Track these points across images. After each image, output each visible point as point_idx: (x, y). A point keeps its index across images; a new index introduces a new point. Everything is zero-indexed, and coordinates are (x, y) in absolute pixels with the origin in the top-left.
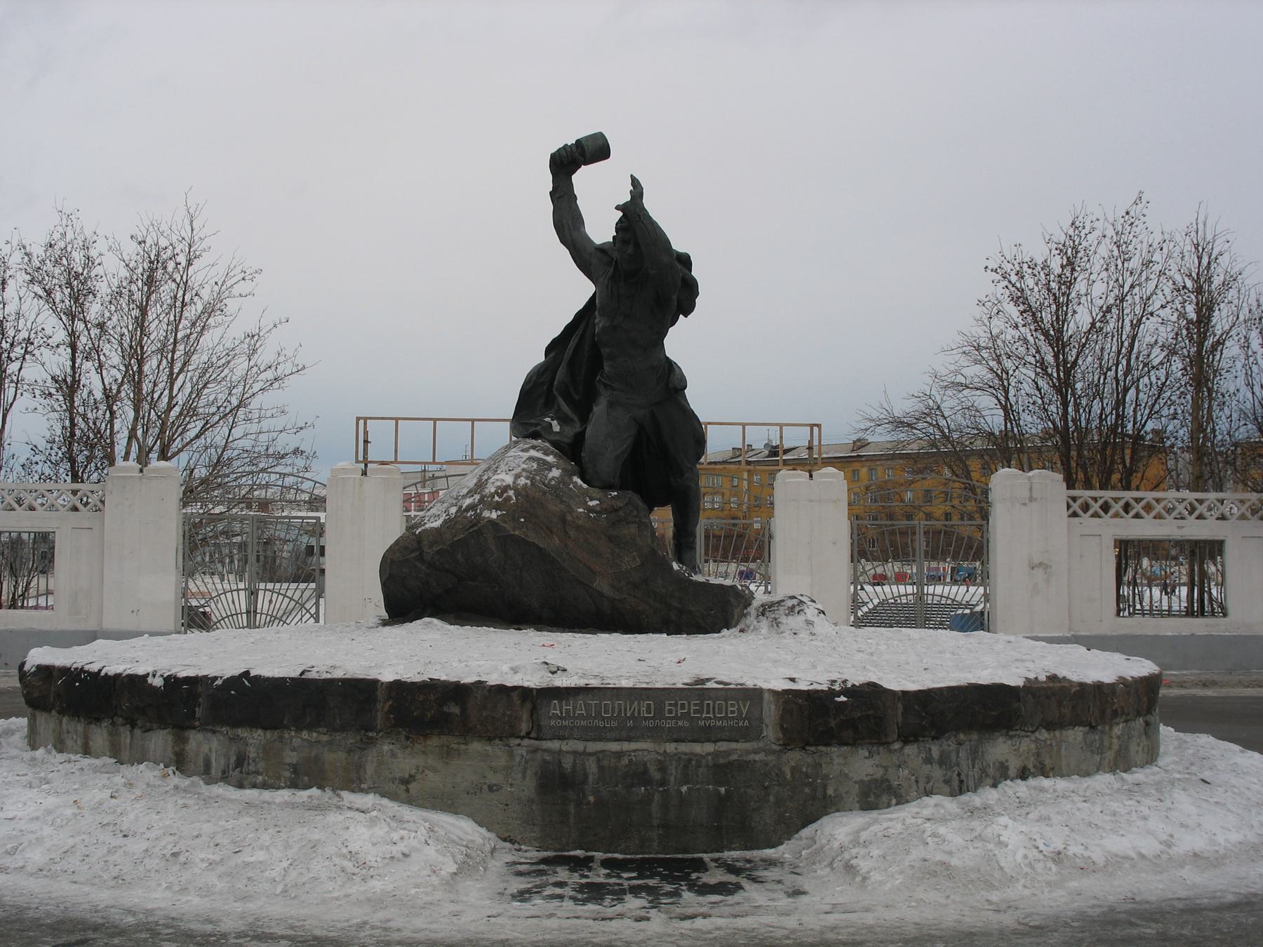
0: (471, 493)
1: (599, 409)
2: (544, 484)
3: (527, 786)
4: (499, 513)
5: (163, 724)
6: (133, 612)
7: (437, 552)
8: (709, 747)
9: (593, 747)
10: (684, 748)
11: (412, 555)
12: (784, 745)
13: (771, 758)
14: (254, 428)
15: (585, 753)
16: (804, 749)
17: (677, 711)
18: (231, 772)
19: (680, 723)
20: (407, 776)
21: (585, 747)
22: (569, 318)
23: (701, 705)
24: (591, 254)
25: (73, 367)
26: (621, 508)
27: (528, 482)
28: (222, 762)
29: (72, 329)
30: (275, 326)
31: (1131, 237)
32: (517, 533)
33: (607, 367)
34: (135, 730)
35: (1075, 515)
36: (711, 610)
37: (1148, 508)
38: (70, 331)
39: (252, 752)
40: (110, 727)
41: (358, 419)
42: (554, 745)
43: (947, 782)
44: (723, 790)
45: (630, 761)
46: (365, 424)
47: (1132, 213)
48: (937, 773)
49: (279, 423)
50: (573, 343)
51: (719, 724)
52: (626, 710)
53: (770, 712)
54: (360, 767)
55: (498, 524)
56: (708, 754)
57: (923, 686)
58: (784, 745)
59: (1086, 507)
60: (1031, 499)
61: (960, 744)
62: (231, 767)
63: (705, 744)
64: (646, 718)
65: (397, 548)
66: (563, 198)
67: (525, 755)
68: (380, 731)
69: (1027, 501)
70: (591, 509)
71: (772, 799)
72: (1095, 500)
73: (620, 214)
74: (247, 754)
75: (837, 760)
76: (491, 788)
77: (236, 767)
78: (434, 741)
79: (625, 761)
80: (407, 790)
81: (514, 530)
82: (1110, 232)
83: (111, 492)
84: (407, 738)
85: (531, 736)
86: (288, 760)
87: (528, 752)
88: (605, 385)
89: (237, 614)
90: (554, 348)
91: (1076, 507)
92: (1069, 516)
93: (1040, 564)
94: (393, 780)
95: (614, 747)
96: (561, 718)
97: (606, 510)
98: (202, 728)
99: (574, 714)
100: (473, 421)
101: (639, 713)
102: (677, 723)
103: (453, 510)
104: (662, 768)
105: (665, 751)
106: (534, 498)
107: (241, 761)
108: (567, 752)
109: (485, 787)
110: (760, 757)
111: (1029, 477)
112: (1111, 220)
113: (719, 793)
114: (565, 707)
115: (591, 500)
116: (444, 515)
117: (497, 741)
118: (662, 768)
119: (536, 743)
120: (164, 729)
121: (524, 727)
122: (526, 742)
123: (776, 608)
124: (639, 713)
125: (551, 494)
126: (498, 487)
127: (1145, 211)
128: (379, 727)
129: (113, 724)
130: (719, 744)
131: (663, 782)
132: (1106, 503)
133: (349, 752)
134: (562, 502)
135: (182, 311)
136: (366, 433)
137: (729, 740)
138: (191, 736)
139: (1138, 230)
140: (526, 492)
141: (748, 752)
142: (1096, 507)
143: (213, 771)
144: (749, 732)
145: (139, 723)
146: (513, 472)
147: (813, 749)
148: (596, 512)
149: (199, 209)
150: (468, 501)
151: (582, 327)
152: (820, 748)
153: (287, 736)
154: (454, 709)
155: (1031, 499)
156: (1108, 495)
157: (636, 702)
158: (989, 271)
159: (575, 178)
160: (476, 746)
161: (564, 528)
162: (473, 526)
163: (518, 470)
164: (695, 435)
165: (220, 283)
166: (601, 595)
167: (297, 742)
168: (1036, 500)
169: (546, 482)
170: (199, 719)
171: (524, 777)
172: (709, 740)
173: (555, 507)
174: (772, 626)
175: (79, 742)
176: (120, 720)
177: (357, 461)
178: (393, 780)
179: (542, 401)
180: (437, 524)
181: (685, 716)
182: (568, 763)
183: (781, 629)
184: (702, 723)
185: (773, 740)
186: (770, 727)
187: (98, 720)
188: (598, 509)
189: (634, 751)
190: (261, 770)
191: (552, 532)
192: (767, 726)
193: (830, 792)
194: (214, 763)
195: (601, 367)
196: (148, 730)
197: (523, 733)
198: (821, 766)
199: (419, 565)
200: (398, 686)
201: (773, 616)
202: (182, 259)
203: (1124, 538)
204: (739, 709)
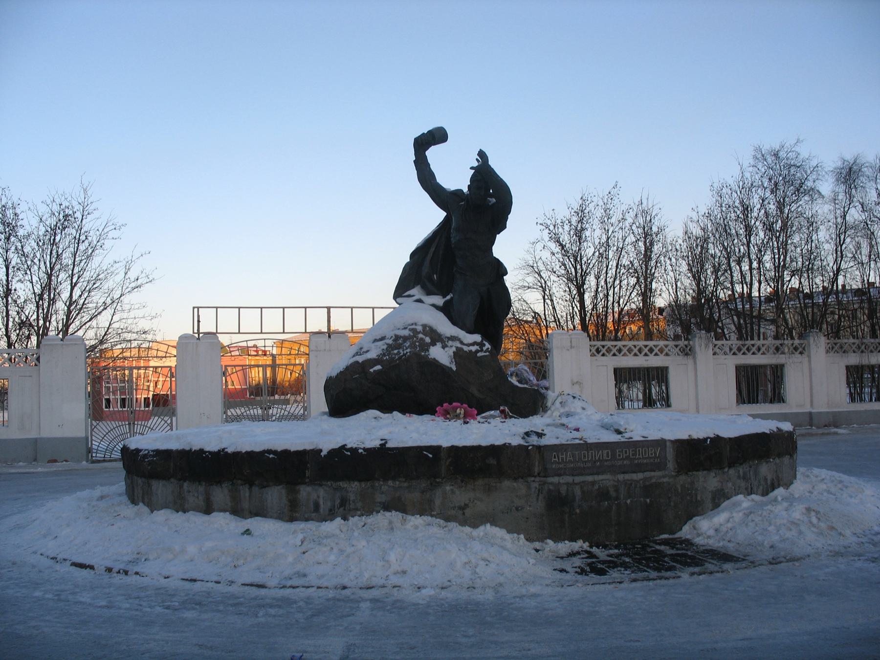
3: (538, 506)
5: (278, 481)
6: (59, 426)
8: (640, 476)
9: (578, 479)
10: (627, 477)
12: (677, 472)
13: (672, 480)
14: (125, 315)
15: (575, 484)
16: (687, 473)
17: (623, 455)
18: (336, 511)
19: (625, 462)
20: (463, 504)
21: (573, 480)
25: (7, 280)
28: (329, 504)
29: (6, 257)
30: (142, 255)
31: (612, 206)
34: (253, 488)
35: (593, 355)
37: (630, 351)
38: (5, 258)
39: (352, 497)
40: (230, 487)
41: (194, 308)
42: (555, 480)
43: (746, 489)
44: (648, 500)
45: (599, 486)
47: (612, 193)
48: (743, 484)
49: (140, 313)
51: (645, 461)
52: (595, 456)
53: (670, 454)
54: (431, 501)
56: (641, 480)
58: (677, 472)
59: (598, 351)
60: (571, 347)
61: (751, 467)
62: (336, 507)
63: (638, 474)
64: (606, 461)
67: (538, 487)
68: (444, 478)
71: (672, 504)
72: (603, 347)
74: (348, 497)
75: (701, 479)
76: (517, 509)
77: (341, 506)
78: (480, 482)
79: (596, 487)
80: (464, 514)
82: (600, 203)
83: (44, 354)
84: (462, 481)
85: (541, 475)
86: (379, 500)
87: (540, 485)
89: (112, 430)
91: (594, 350)
93: (577, 382)
94: (454, 508)
95: (590, 478)
96: (559, 463)
98: (313, 482)
99: (566, 460)
101: (603, 458)
102: (623, 463)
104: (617, 490)
105: (618, 479)
107: (344, 502)
108: (563, 484)
109: (514, 508)
110: (666, 480)
112: (601, 196)
113: (647, 502)
114: (560, 456)
117: (520, 480)
118: (617, 490)
119: (544, 479)
120: (279, 485)
121: (536, 470)
122: (537, 479)
124: (603, 458)
127: (618, 192)
128: (443, 475)
129: (233, 484)
130: (646, 473)
131: (617, 498)
133: (423, 492)
135: (78, 246)
136: (198, 316)
137: (651, 471)
138: (302, 489)
139: (615, 202)
141: (660, 477)
142: (614, 350)
143: (321, 510)
144: (660, 466)
145: (257, 482)
147: (690, 473)
149: (90, 185)
151: (436, 241)
152: (694, 473)
153: (377, 484)
154: (492, 461)
155: (571, 347)
157: (600, 452)
158: (539, 225)
159: (427, 153)
160: (507, 483)
164: (506, 302)
165: (101, 230)
167: (385, 488)
168: (574, 347)
170: (308, 478)
171: (537, 499)
172: (641, 472)
175: (200, 498)
176: (239, 482)
178: (454, 508)
181: (628, 458)
182: (563, 490)
185: (672, 469)
186: (671, 462)
187: (219, 483)
189: (602, 480)
190: (359, 508)
192: (669, 461)
193: (699, 498)
194: (322, 506)
196: (265, 487)
197: (536, 474)
198: (694, 483)
200: (453, 449)
202: (78, 215)
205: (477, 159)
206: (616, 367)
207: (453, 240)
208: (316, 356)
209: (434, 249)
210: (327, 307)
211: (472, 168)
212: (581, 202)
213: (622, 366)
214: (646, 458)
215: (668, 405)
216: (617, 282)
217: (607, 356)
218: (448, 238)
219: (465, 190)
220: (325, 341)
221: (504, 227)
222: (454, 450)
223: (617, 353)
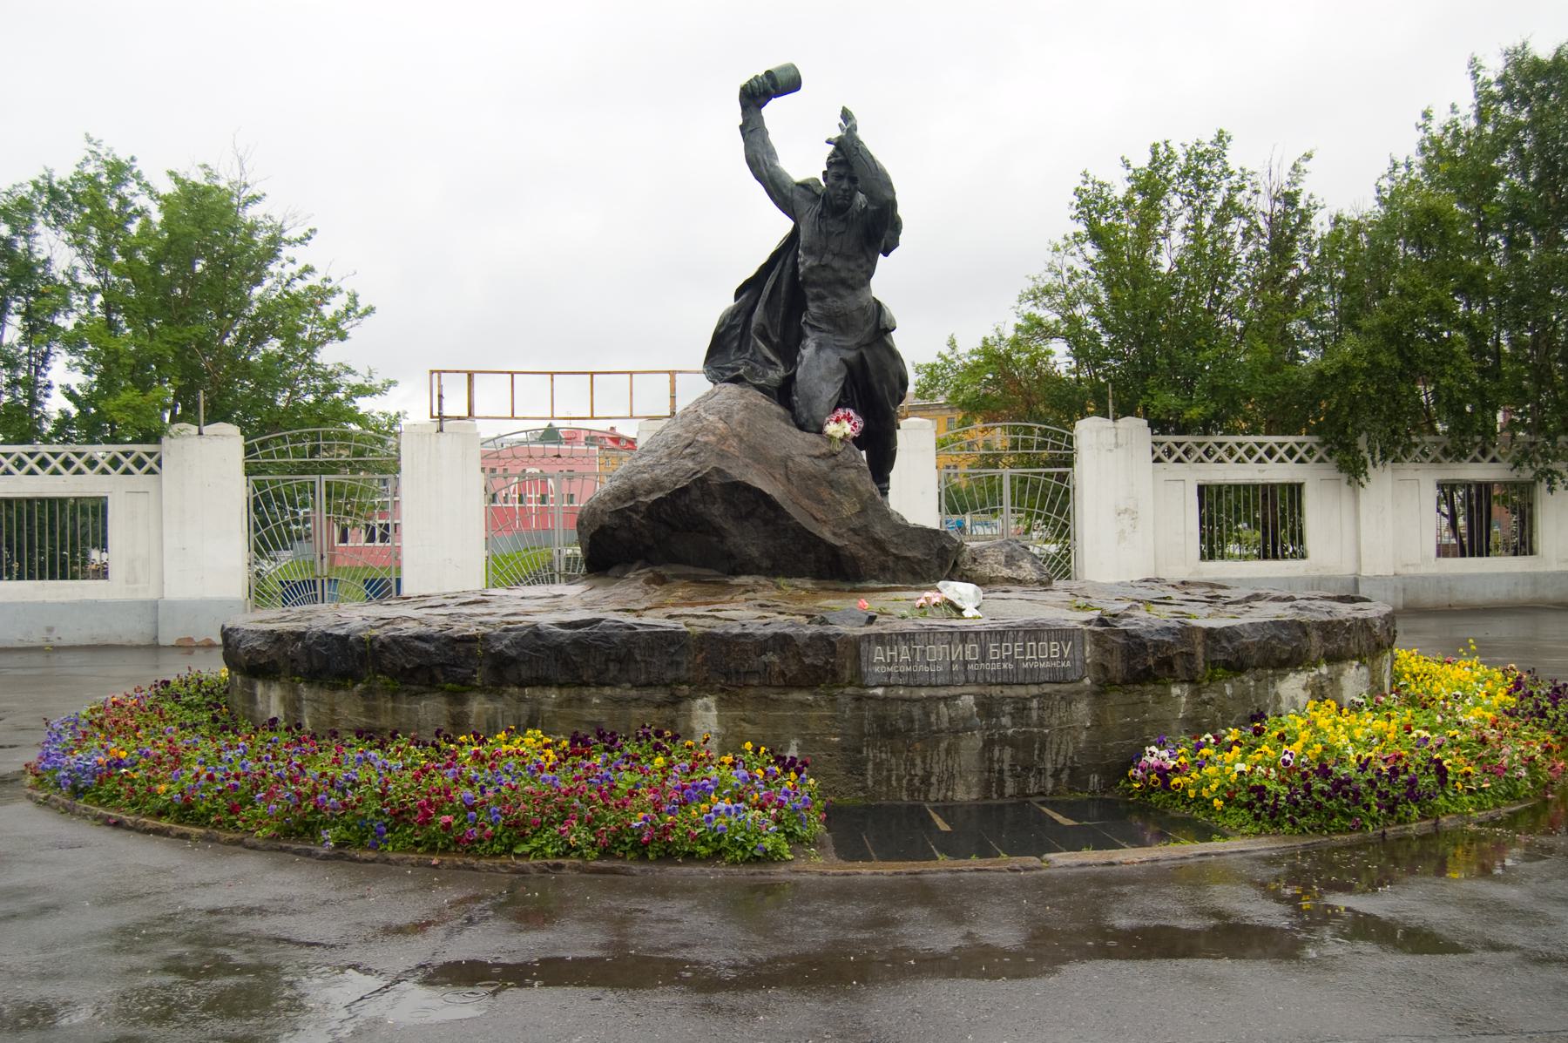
1: (808, 351)
9: (1008, 692)
19: (1005, 666)
22: (763, 258)
23: (1025, 648)
33: (813, 308)
35: (1158, 460)
46: (439, 378)
51: (1042, 665)
59: (1170, 453)
60: (1117, 445)
66: (752, 130)
73: (832, 147)
88: (812, 327)
90: (749, 289)
91: (1159, 451)
92: (1154, 462)
100: (592, 374)
114: (889, 653)
136: (440, 387)
151: (778, 267)
155: (1117, 445)
156: (1251, 440)
159: (764, 110)
162: (695, 474)
177: (432, 417)
179: (736, 344)
184: (1025, 666)
195: (806, 308)
204: (1061, 649)
206: (1201, 483)
207: (801, 269)
210: (669, 372)
211: (829, 142)
214: (1042, 660)
218: (795, 265)
222: (708, 639)
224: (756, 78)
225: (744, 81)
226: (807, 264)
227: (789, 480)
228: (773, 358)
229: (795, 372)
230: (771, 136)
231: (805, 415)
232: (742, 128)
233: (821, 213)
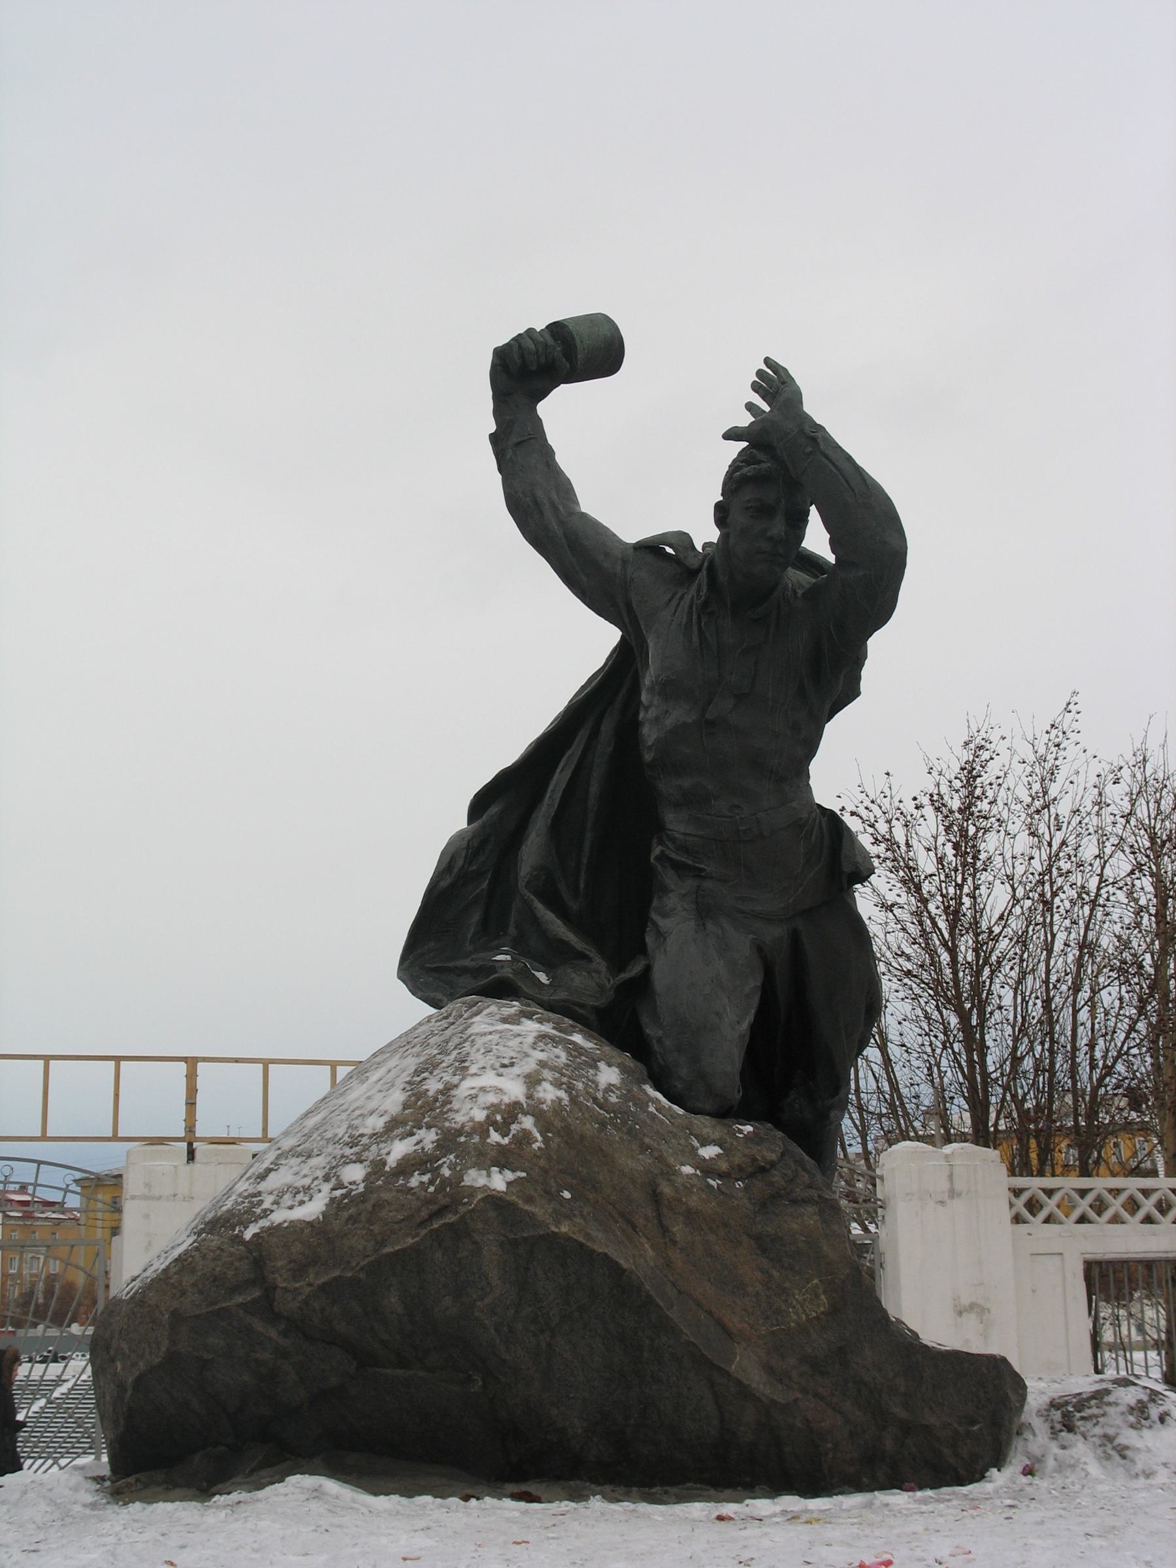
0: (395, 1127)
2: (595, 1100)
4: (510, 1176)
7: (323, 1288)
11: (240, 1299)
24: (625, 562)
26: (773, 1164)
27: (562, 1094)
32: (564, 1229)
33: (676, 823)
35: (1017, 1219)
36: (973, 1422)
37: (1132, 1206)
50: (560, 779)
55: (511, 1204)
57: (318, 1494)
59: (1033, 1206)
60: (953, 1193)
65: (188, 1280)
69: (946, 1197)
70: (707, 1168)
72: (1049, 1193)
81: (558, 1223)
88: (679, 867)
93: (972, 1307)
97: (740, 1168)
103: (355, 1174)
106: (583, 1137)
111: (947, 1156)
115: (703, 1145)
116: (326, 1187)
123: (1095, 1411)
125: (615, 1126)
126: (493, 1108)
132: (1099, 1199)
134: (644, 1148)
140: (563, 1119)
146: (516, 1070)
148: (721, 1176)
150: (399, 1150)
155: (953, 1193)
161: (659, 1216)
163: (529, 1066)
166: (745, 1392)
168: (959, 1195)
169: (599, 1095)
173: (633, 1162)
174: (1108, 1457)
179: (476, 917)
180: (313, 1209)
183: (1139, 1466)
188: (724, 1166)
191: (634, 1227)
199: (258, 1325)
201: (1098, 1430)
203: (1098, 1257)
205: (750, 407)
206: (1089, 1257)
207: (650, 734)
208: (147, 1216)
209: (568, 774)
210: (184, 1059)
211: (732, 435)
212: (967, 756)
213: (1108, 1257)
215: (120, 1176)
216: (1084, 994)
217: (1061, 1223)
219: (705, 533)
220: (175, 1167)
221: (852, 692)
223: (1092, 1214)
224: (530, 331)
225: (503, 340)
226: (669, 722)
227: (665, 1230)
228: (571, 937)
229: (648, 969)
230: (558, 458)
231: (684, 1072)
232: (494, 438)
233: (706, 604)
